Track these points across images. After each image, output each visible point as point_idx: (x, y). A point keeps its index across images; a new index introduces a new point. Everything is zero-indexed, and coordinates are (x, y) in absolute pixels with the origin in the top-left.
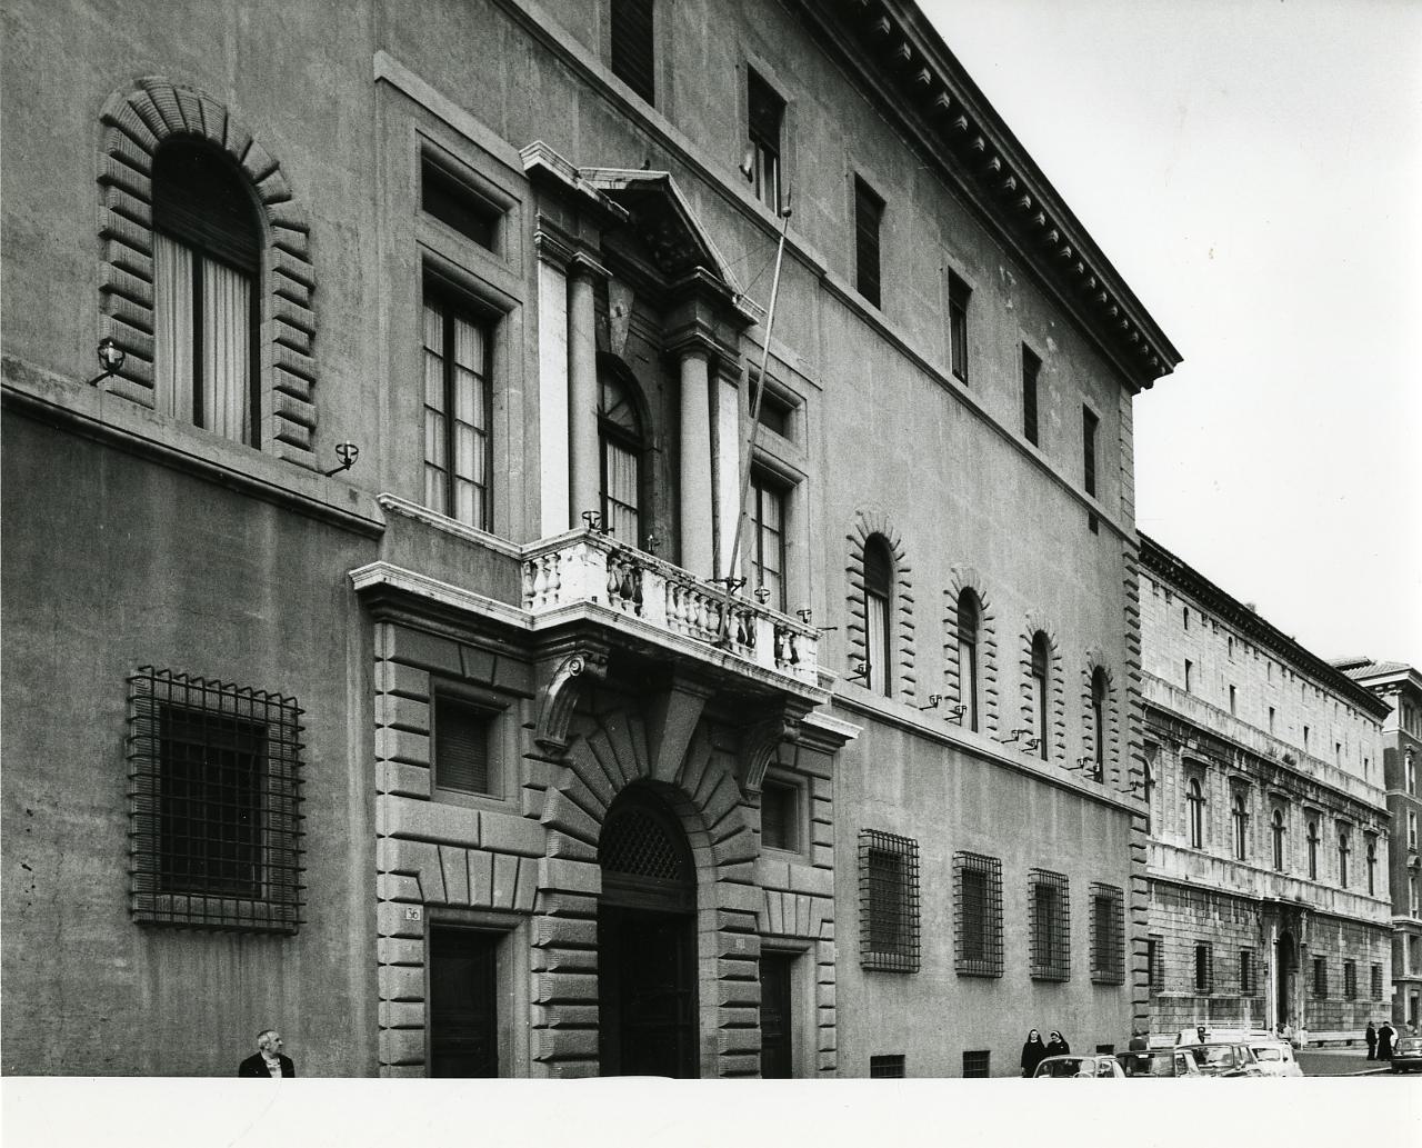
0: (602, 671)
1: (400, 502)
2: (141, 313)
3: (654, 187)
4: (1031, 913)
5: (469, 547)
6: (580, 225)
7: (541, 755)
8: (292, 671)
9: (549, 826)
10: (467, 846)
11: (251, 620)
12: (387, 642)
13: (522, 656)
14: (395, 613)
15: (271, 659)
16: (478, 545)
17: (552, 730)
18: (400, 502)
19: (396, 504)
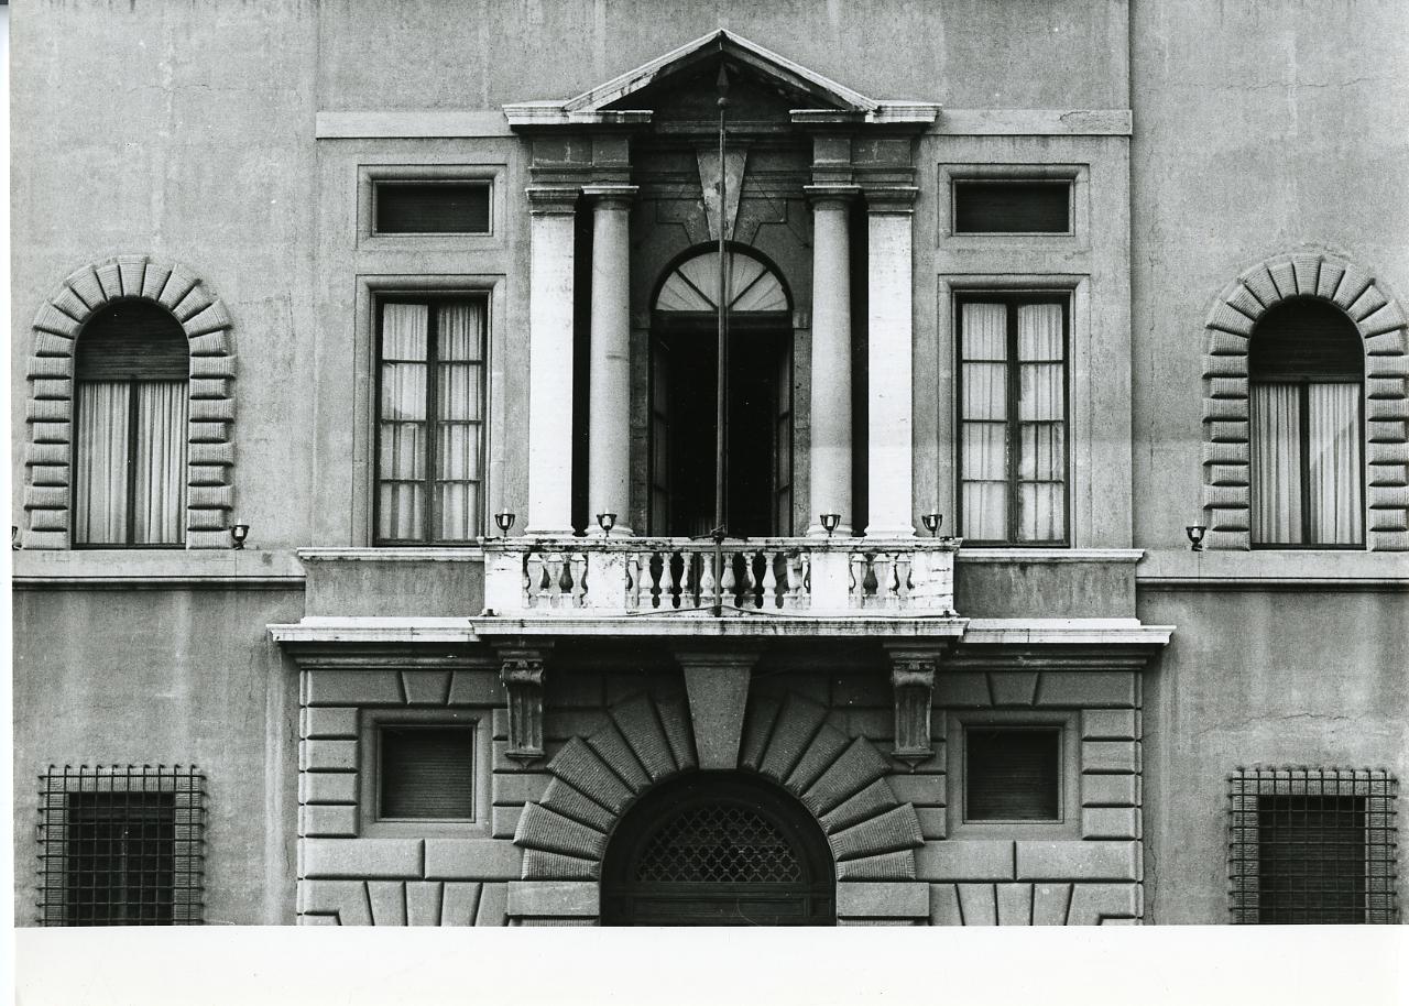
0: (537, 676)
1: (315, 551)
2: (54, 474)
3: (704, 54)
4: (1234, 904)
5: (415, 567)
6: (594, 146)
7: (515, 768)
8: (204, 737)
9: (522, 845)
10: (404, 879)
11: (162, 701)
12: (308, 687)
13: (487, 664)
14: (309, 661)
15: (183, 730)
16: (425, 561)
17: (519, 740)
18: (315, 551)
19: (313, 554)
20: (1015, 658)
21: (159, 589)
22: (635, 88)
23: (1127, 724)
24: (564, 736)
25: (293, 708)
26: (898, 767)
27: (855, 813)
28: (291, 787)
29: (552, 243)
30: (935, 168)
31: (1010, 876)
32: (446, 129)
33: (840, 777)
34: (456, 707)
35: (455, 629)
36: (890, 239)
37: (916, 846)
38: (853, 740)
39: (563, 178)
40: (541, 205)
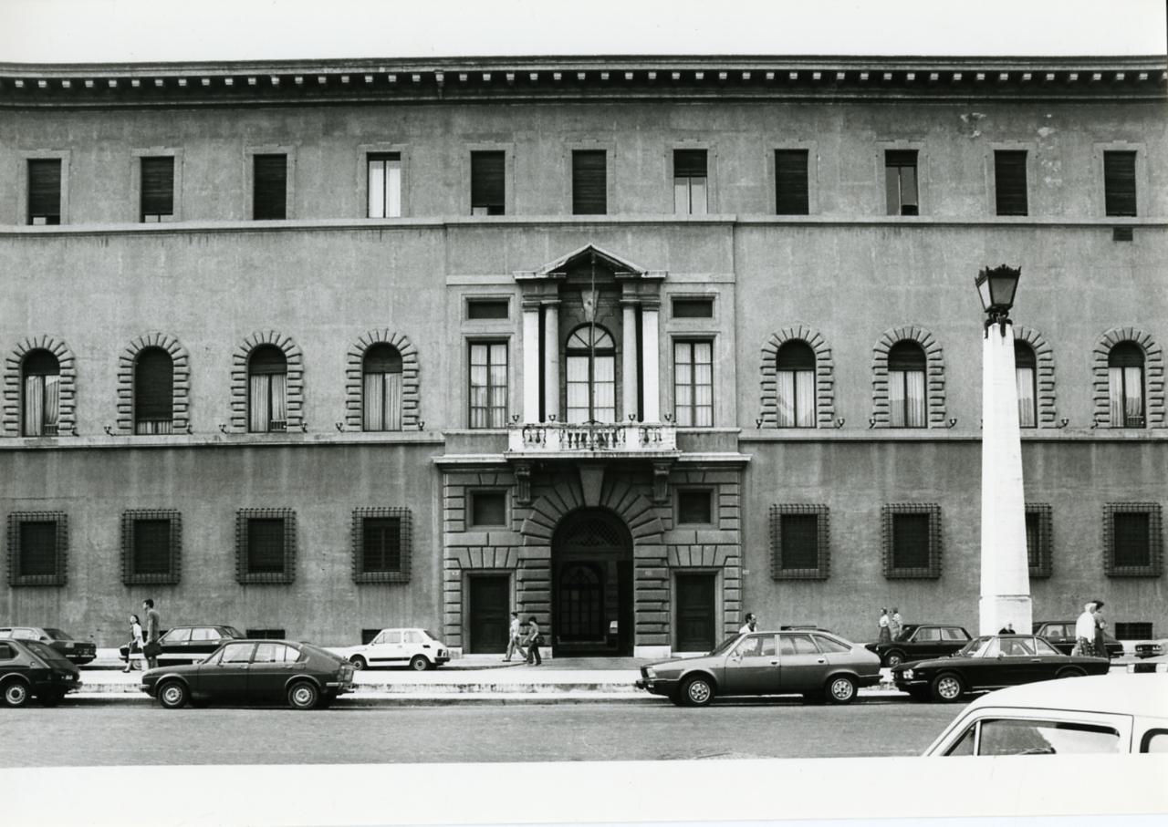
23: (735, 489)
25: (442, 487)
28: (441, 515)
29: (531, 320)
30: (666, 294)
32: (494, 282)
33: (636, 509)
35: (498, 458)
36: (650, 319)
37: (662, 533)
40: (527, 308)
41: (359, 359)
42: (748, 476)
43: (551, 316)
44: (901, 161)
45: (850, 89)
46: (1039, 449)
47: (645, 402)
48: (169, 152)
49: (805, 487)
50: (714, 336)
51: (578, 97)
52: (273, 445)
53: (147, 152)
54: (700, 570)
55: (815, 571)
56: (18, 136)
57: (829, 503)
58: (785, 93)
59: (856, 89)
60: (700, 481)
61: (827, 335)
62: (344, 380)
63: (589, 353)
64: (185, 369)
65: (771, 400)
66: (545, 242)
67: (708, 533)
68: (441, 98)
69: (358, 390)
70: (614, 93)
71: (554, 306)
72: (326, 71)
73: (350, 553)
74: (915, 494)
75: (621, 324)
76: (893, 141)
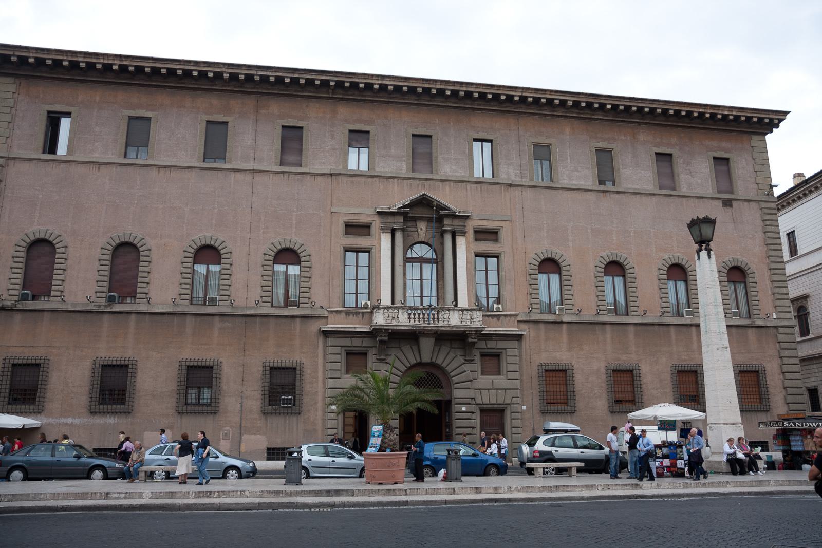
20: (491, 337)
21: (293, 317)
22: (406, 204)
23: (516, 352)
24: (390, 354)
25: (325, 346)
26: (467, 362)
27: (458, 372)
28: (324, 366)
29: (386, 240)
30: (470, 226)
31: (492, 388)
32: (362, 213)
33: (454, 364)
34: (364, 347)
35: (366, 328)
36: (461, 242)
37: (471, 381)
38: (456, 356)
39: (388, 224)
40: (383, 230)
41: (191, 255)
42: (523, 343)
43: (399, 236)
44: (664, 158)
45: (574, 111)
46: (734, 330)
47: (467, 293)
48: (149, 114)
49: (557, 352)
50: (500, 254)
51: (415, 102)
52: (289, 315)
53: (536, 140)
54: (496, 406)
55: (567, 408)
56: (41, 96)
57: (574, 363)
58: (537, 110)
59: (577, 111)
60: (494, 347)
61: (566, 255)
62: (97, 265)
63: (421, 261)
64: (64, 256)
65: (533, 293)
66: (395, 186)
67: (500, 380)
68: (331, 96)
69: (189, 276)
70: (437, 101)
71: (403, 230)
72: (260, 73)
73: (260, 392)
74: (624, 357)
75: (442, 244)
76: (598, 142)
